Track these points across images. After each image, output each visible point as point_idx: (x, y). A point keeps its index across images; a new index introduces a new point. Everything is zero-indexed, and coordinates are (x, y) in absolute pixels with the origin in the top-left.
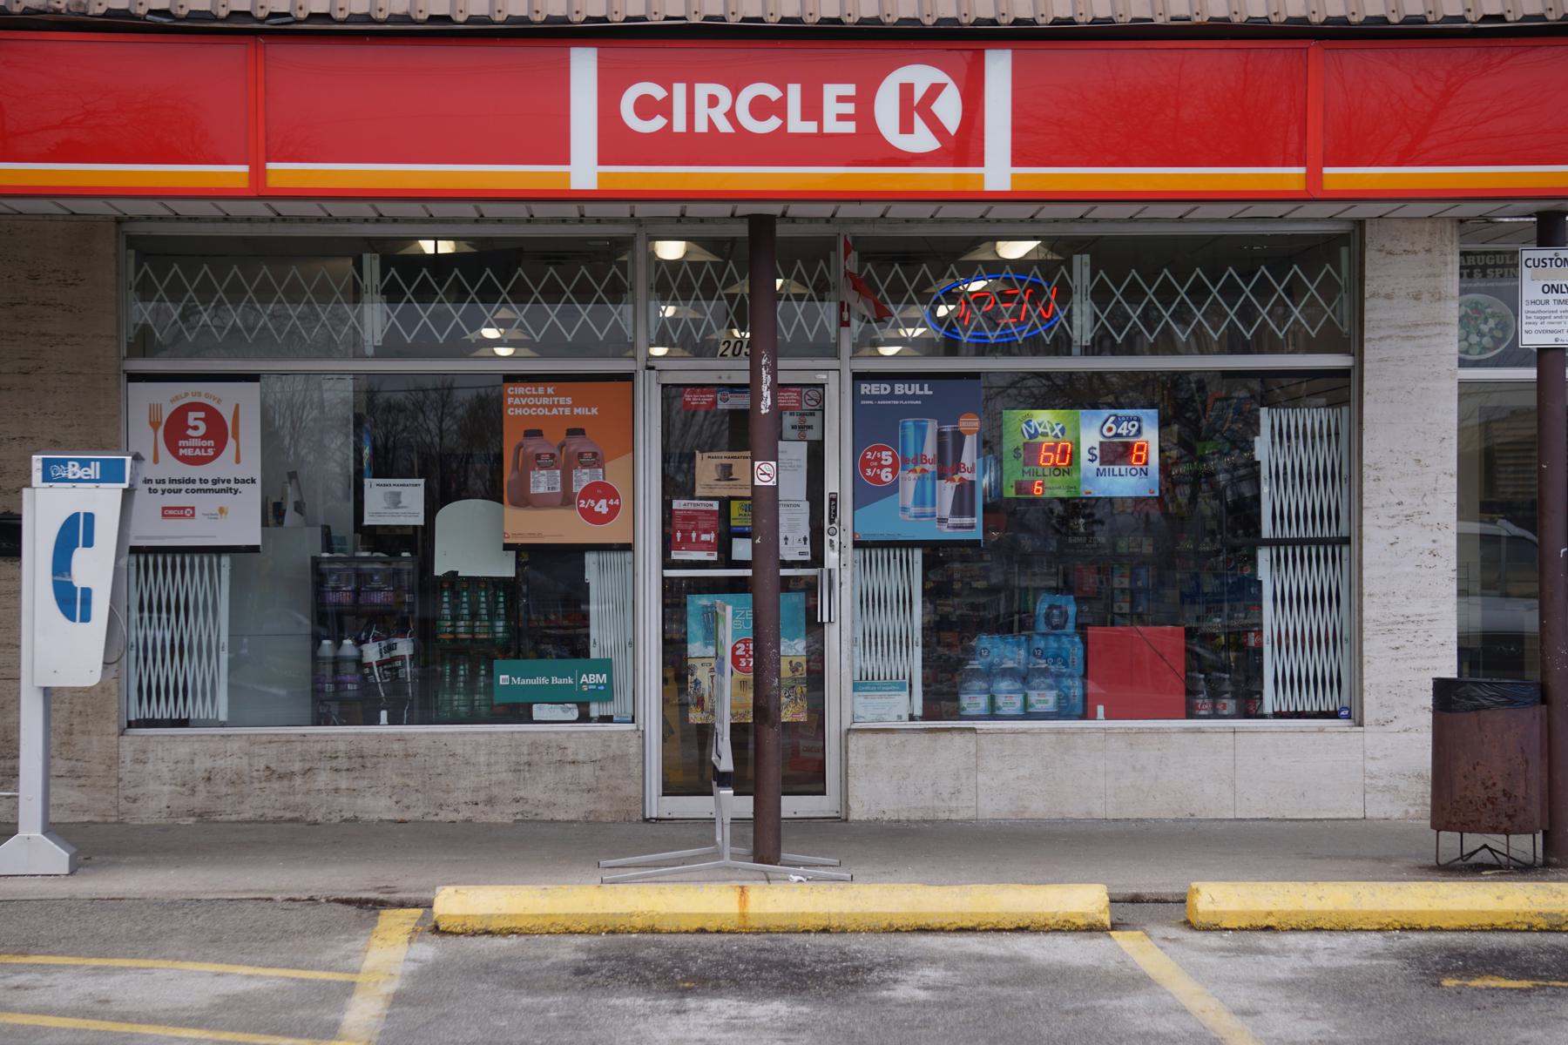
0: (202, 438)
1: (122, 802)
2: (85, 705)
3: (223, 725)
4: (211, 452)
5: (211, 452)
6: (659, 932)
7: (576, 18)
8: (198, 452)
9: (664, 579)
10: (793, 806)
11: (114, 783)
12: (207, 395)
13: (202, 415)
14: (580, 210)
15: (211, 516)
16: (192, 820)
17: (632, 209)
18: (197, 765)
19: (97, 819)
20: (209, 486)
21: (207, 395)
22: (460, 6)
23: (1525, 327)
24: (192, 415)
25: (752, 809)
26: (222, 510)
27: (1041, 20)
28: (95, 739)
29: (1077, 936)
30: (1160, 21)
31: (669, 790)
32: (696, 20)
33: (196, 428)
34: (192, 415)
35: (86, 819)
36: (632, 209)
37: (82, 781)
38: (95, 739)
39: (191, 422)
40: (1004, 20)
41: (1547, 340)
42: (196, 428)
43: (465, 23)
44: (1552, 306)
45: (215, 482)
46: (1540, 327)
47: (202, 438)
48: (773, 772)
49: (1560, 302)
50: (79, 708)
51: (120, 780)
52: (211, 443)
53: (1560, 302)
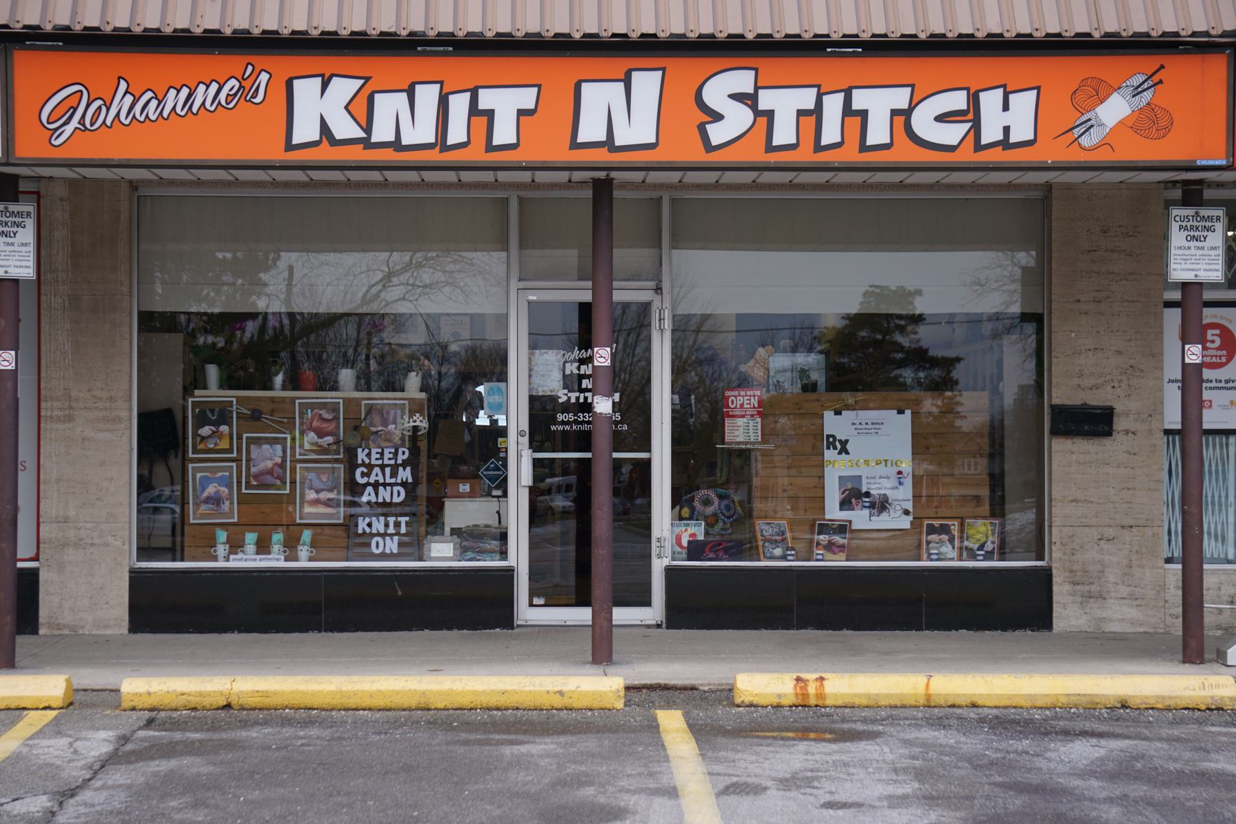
0: (1218, 349)
1: (1168, 618)
2: (1140, 546)
3: (1229, 562)
4: (1224, 359)
5: (1224, 359)
6: (959, 707)
7: (604, 34)
8: (1214, 360)
9: (649, 451)
10: (622, 615)
11: (1162, 604)
12: (1222, 318)
13: (1218, 332)
14: (495, 176)
15: (1225, 407)
16: (1219, 633)
17: (533, 175)
18: (1223, 591)
19: (1151, 630)
20: (1223, 384)
21: (1222, 318)
22: (79, 19)
23: (1173, 266)
24: (1210, 332)
25: (590, 618)
26: (1232, 403)
27: (1007, 35)
28: (1148, 572)
29: (364, 705)
30: (923, 36)
31: (647, 603)
32: (577, 36)
33: (1213, 342)
34: (1210, 332)
35: (1142, 630)
36: (533, 175)
37: (1139, 602)
38: (1148, 572)
39: (1209, 337)
40: (1154, 34)
41: (1188, 276)
42: (1213, 342)
43: (1220, 36)
44: (1193, 251)
45: (1227, 382)
46: (1184, 266)
47: (1218, 349)
48: (601, 586)
49: (1199, 248)
50: (1136, 548)
51: (1166, 602)
52: (1224, 353)
53: (1199, 248)
